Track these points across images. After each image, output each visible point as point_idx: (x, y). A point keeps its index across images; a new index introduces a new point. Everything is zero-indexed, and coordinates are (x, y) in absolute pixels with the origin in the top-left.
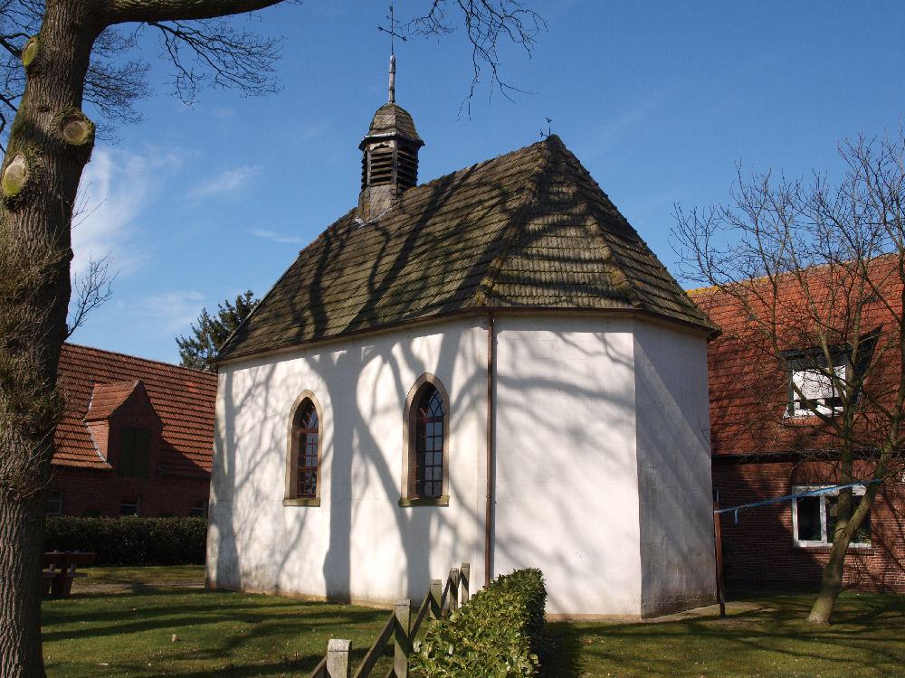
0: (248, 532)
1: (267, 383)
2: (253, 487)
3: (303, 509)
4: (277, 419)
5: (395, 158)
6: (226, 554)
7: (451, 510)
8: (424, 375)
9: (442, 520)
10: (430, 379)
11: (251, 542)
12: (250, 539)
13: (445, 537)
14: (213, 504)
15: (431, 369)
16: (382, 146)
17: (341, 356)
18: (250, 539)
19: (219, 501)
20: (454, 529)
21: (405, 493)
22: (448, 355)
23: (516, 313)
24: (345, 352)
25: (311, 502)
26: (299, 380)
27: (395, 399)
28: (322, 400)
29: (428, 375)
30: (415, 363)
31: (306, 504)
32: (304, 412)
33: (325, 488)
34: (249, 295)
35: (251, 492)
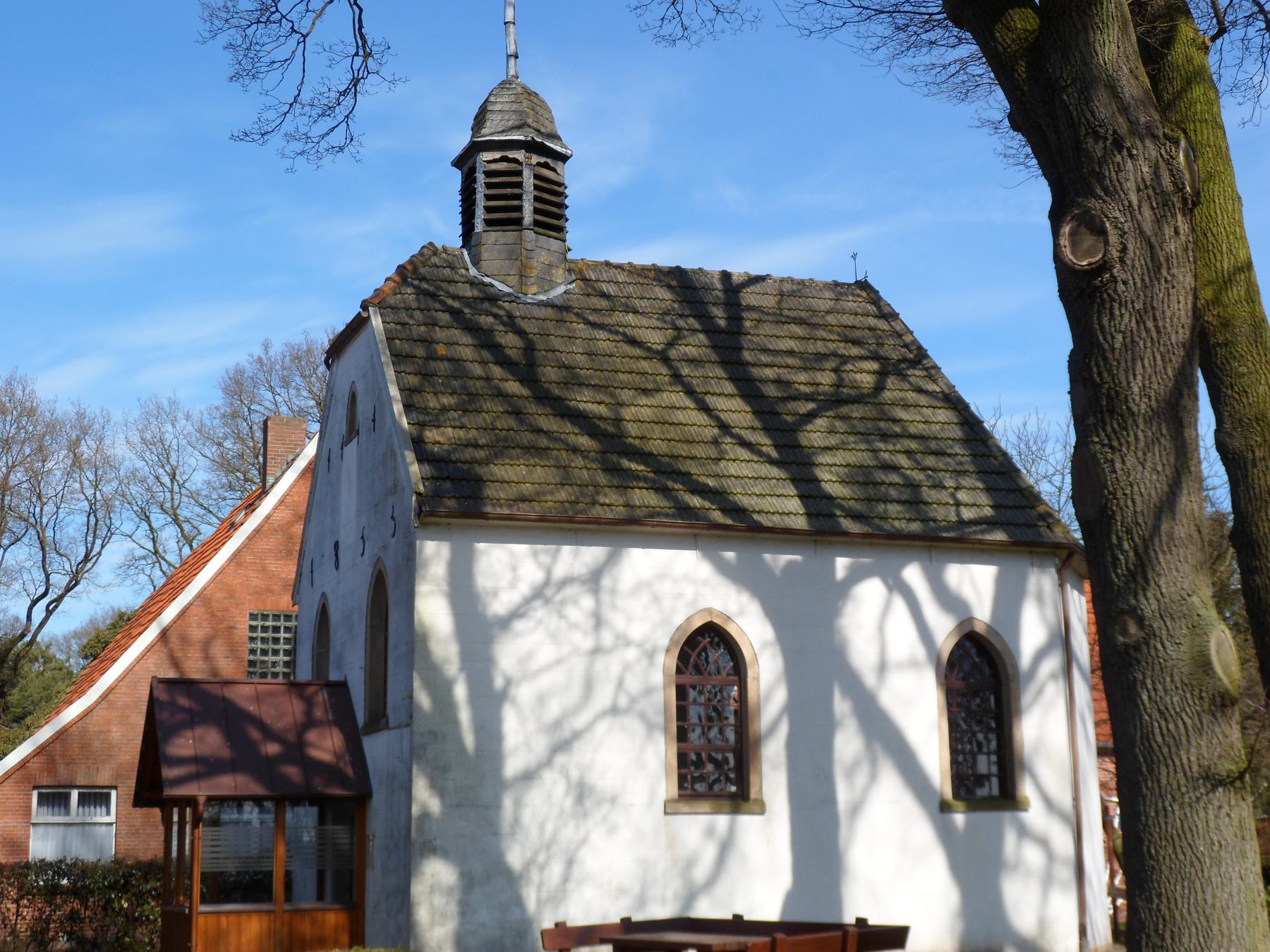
0: (556, 869)
1: (593, 580)
2: (567, 777)
3: (722, 821)
4: (631, 654)
5: (512, 181)
6: (485, 916)
7: (1035, 815)
8: (970, 620)
9: (1023, 832)
10: (980, 629)
11: (571, 886)
12: (566, 879)
13: (1033, 855)
14: (425, 815)
15: (983, 612)
16: (546, 166)
17: (790, 564)
18: (566, 879)
19: (448, 807)
20: (1043, 843)
21: (948, 792)
22: (1008, 599)
23: (875, 541)
24: (798, 558)
25: (746, 806)
26: (689, 591)
27: (920, 652)
28: (753, 629)
29: (976, 622)
30: (948, 600)
31: (736, 811)
32: (706, 654)
33: (773, 779)
34: (266, 347)
35: (560, 788)
